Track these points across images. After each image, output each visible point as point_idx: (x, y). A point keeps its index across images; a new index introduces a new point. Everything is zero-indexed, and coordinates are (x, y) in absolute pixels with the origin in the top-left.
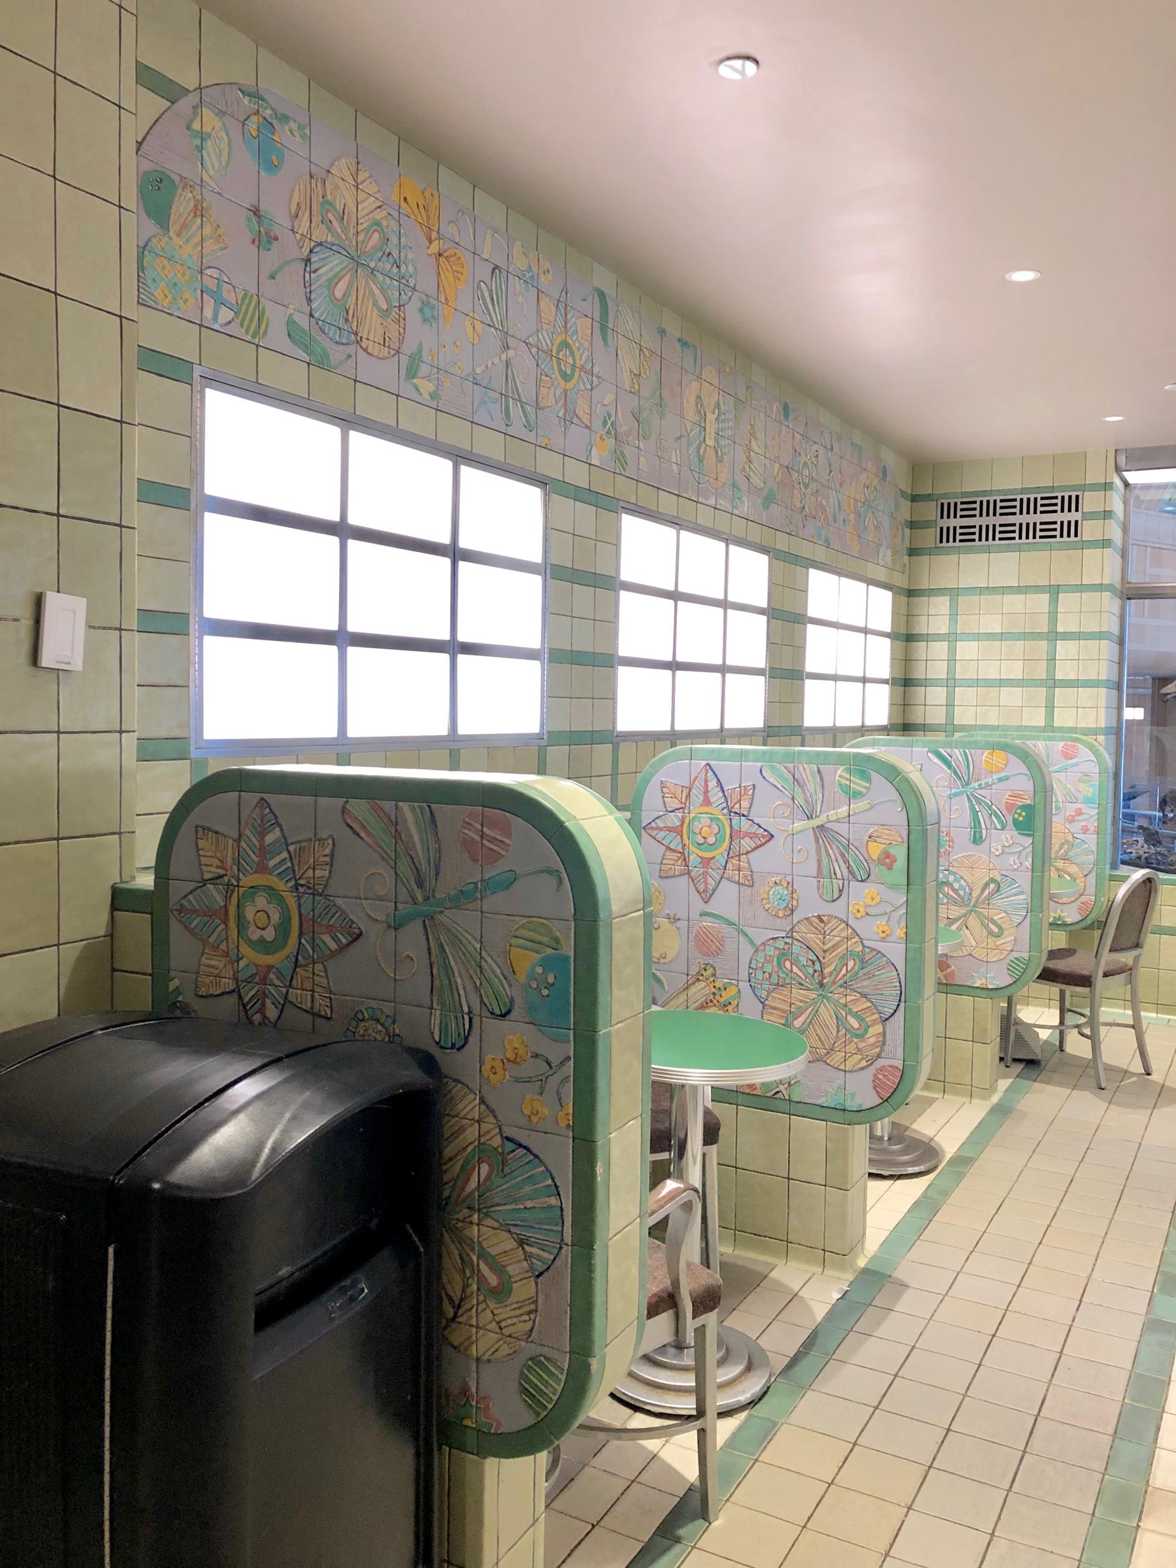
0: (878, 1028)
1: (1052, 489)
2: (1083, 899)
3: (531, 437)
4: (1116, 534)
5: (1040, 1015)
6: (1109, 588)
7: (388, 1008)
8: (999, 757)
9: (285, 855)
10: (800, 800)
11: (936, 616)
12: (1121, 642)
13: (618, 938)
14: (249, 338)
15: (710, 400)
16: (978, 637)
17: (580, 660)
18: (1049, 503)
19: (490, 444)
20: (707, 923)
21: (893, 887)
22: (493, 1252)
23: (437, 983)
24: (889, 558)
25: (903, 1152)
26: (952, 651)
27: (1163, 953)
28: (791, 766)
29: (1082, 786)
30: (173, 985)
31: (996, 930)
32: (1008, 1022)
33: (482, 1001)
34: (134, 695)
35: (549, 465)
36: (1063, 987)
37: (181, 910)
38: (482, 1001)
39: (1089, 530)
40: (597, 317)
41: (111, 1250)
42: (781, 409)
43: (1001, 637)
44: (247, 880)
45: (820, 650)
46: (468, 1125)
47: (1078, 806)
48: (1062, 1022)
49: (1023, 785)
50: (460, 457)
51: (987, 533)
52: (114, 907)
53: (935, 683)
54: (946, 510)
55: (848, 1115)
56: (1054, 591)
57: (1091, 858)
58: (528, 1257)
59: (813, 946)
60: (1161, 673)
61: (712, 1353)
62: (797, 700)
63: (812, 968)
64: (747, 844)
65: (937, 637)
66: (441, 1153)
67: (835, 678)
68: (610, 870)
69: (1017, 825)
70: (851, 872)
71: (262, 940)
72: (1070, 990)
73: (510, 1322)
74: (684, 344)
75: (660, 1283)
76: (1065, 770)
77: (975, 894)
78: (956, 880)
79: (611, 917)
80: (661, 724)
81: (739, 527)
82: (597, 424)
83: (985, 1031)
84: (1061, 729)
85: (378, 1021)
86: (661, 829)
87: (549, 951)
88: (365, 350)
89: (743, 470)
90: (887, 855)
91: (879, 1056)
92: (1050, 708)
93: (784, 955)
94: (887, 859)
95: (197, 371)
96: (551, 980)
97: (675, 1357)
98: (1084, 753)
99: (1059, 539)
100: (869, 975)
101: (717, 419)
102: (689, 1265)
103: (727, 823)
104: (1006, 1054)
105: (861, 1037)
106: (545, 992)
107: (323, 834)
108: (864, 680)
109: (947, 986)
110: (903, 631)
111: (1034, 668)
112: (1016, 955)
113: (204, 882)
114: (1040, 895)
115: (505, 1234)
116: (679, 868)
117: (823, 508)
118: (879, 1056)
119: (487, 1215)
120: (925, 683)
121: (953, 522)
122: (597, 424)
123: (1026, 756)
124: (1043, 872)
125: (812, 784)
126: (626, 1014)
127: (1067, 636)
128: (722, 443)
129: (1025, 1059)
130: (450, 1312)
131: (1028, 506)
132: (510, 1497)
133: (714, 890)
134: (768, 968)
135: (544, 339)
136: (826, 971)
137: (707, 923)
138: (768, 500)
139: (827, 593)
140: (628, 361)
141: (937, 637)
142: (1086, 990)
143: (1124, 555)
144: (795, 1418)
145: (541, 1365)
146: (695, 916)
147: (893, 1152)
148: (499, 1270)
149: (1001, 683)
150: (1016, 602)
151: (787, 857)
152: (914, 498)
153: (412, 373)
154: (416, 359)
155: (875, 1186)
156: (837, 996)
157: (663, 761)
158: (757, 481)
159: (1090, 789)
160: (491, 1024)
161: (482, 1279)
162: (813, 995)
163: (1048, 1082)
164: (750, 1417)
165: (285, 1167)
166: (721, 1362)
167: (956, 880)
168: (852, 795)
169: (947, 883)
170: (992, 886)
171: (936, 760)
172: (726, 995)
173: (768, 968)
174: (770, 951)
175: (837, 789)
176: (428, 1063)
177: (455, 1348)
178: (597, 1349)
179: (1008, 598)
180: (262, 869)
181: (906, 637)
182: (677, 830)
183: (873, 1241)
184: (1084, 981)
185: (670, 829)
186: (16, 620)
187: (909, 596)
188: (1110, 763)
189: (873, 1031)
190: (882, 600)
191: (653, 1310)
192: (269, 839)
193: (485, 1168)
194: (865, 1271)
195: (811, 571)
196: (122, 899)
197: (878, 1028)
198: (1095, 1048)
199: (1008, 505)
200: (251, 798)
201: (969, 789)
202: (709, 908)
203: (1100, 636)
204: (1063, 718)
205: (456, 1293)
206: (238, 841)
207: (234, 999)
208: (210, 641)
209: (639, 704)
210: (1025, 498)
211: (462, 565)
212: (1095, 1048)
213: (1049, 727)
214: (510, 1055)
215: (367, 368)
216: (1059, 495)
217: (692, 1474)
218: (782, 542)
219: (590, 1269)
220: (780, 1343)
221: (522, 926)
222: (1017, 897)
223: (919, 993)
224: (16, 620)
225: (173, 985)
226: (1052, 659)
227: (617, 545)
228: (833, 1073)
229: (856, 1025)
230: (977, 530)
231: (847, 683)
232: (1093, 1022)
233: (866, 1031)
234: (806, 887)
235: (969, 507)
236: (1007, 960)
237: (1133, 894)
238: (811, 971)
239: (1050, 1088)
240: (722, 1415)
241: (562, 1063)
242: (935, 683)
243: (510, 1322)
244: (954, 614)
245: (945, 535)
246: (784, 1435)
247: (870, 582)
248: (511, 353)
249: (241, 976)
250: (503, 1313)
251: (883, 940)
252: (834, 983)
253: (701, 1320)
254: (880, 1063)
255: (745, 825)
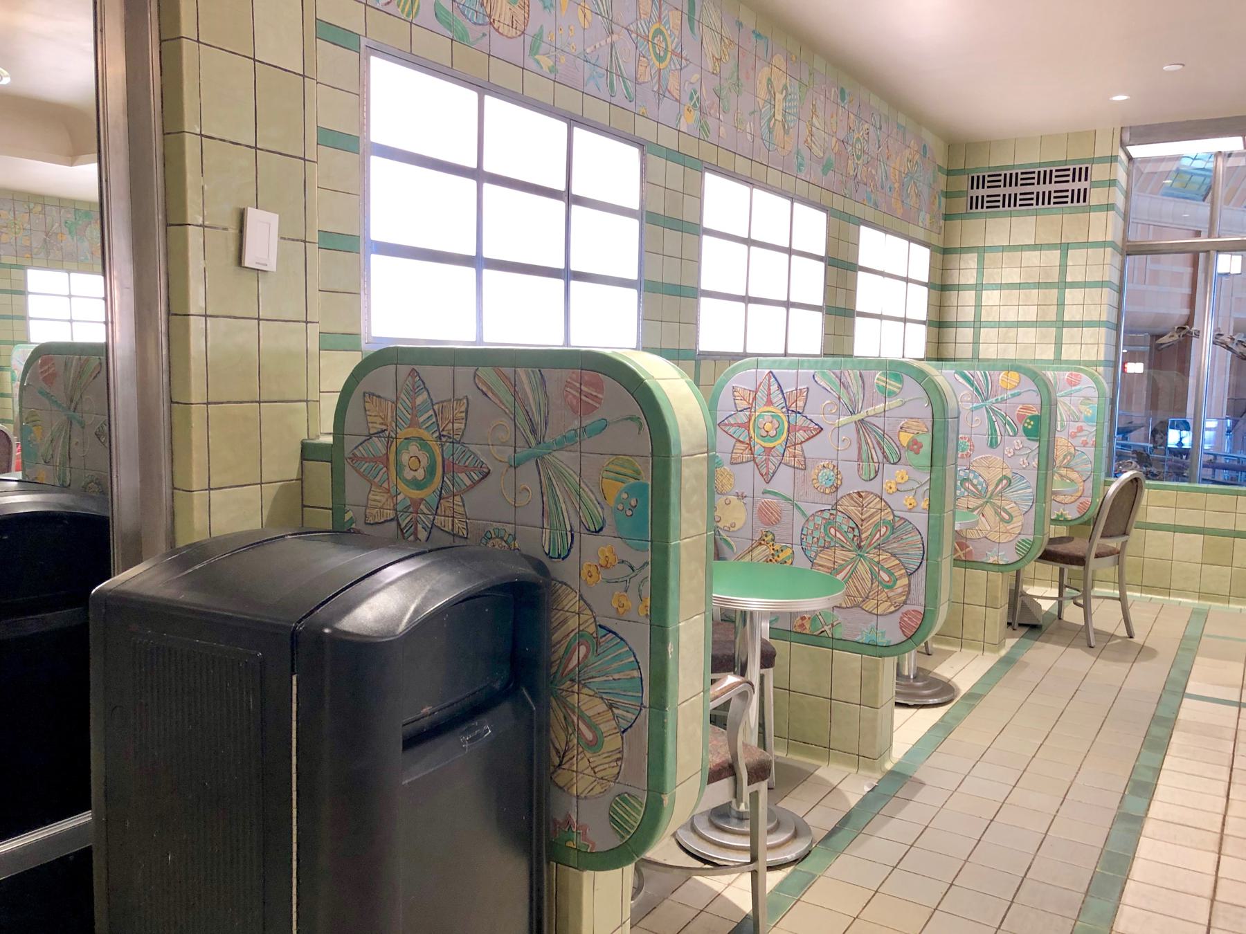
0: (905, 581)
1: (1066, 162)
2: (1082, 500)
3: (631, 106)
4: (1120, 201)
5: (1043, 593)
6: (1112, 244)
7: (509, 528)
8: (1014, 376)
9: (431, 412)
10: (845, 399)
11: (966, 270)
12: (1120, 291)
13: (686, 472)
14: (404, 16)
15: (778, 84)
16: (1000, 286)
17: (669, 291)
18: (1063, 174)
19: (599, 111)
20: (769, 499)
21: (918, 468)
22: (590, 713)
23: (546, 507)
24: (928, 222)
25: (924, 688)
26: (979, 298)
27: (1146, 544)
28: (838, 372)
29: (1082, 408)
30: (347, 517)
31: (1006, 517)
32: (1016, 598)
33: (581, 521)
34: (316, 298)
35: (644, 129)
36: (1062, 565)
37: (354, 458)
38: (581, 521)
39: (1096, 197)
40: (686, 10)
41: (294, 678)
42: (838, 93)
43: (1019, 286)
44: (402, 433)
45: (869, 293)
46: (570, 618)
47: (1080, 424)
48: (1061, 594)
49: (1031, 399)
50: (573, 121)
51: (1009, 201)
52: (304, 458)
53: (964, 324)
54: (976, 182)
55: (880, 650)
56: (1064, 248)
57: (1089, 467)
58: (616, 717)
59: (853, 516)
60: (1159, 330)
61: (763, 825)
62: (849, 333)
63: (852, 534)
64: (801, 435)
65: (967, 287)
66: (549, 639)
67: (880, 317)
68: (680, 419)
69: (1027, 433)
70: (885, 457)
71: (415, 479)
72: (1068, 568)
73: (601, 767)
74: (758, 36)
75: (721, 756)
76: (1070, 395)
77: (990, 489)
78: (975, 477)
79: (680, 456)
80: (739, 349)
81: (802, 188)
82: (685, 98)
83: (996, 598)
84: (1067, 362)
85: (502, 538)
86: (732, 425)
87: (632, 481)
88: (497, 30)
89: (806, 141)
90: (915, 442)
91: (905, 603)
92: (1059, 344)
93: (830, 523)
94: (915, 446)
95: (364, 42)
96: (633, 502)
97: (737, 825)
98: (1086, 381)
99: (1069, 204)
100: (898, 539)
101: (785, 98)
102: (745, 745)
103: (785, 419)
104: (1014, 618)
105: (891, 588)
106: (629, 513)
107: (459, 395)
108: (905, 320)
109: (965, 562)
110: (938, 282)
111: (1047, 317)
112: (1023, 537)
113: (370, 436)
114: (1043, 492)
115: (597, 701)
116: (747, 456)
117: (873, 177)
118: (905, 603)
119: (585, 686)
120: (956, 324)
121: (981, 192)
122: (685, 98)
123: (1035, 377)
124: (1047, 469)
125: (855, 386)
126: (692, 532)
127: (1074, 285)
128: (789, 118)
129: (1027, 623)
130: (557, 761)
131: (1045, 177)
132: (602, 906)
133: (774, 473)
134: (816, 534)
135: (642, 27)
136: (863, 536)
137: (769, 499)
138: (827, 168)
139: (875, 247)
140: (712, 48)
141: (967, 287)
142: (1081, 568)
143: (1126, 217)
144: (829, 872)
145: (624, 800)
146: (758, 493)
147: (918, 688)
148: (592, 727)
149: (1018, 324)
150: (1032, 258)
151: (834, 446)
152: (949, 173)
153: (534, 50)
154: (538, 37)
155: (899, 712)
156: (872, 555)
157: (734, 371)
158: (817, 151)
159: (1089, 411)
160: (589, 539)
161: (580, 735)
162: (852, 555)
163: (1047, 642)
164: (795, 870)
165: (423, 628)
166: (770, 832)
167: (975, 477)
168: (887, 394)
169: (968, 480)
170: (1004, 482)
171: (961, 380)
172: (783, 556)
173: (816, 534)
174: (819, 521)
175: (876, 389)
176: (540, 567)
177: (561, 788)
178: (668, 786)
179: (1026, 254)
180: (413, 424)
181: (940, 287)
182: (746, 426)
183: (898, 751)
184: (1080, 561)
185: (740, 425)
186: (225, 229)
187: (943, 254)
188: (1107, 388)
189: (899, 583)
190: (921, 256)
191: (715, 775)
192: (419, 401)
193: (583, 649)
194: (891, 773)
195: (862, 228)
196: (309, 452)
197: (905, 581)
198: (1087, 615)
199: (1027, 177)
200: (404, 370)
201: (988, 403)
202: (769, 488)
203: (1101, 284)
204: (1069, 353)
205: (561, 746)
206: (395, 403)
207: (394, 524)
208: (375, 258)
209: (717, 329)
210: (1042, 170)
211: (574, 208)
212: (1087, 615)
213: (1058, 359)
214: (603, 562)
215: (499, 45)
216: (1072, 168)
217: (748, 908)
218: (838, 203)
219: (663, 726)
220: (821, 820)
221: (612, 463)
222: (1024, 492)
223: (939, 552)
224: (225, 229)
225: (347, 517)
226: (1061, 304)
227: (701, 199)
228: (868, 616)
229: (887, 579)
230: (1001, 198)
231: (891, 326)
232: (1086, 596)
233: (895, 583)
234: (849, 470)
235: (995, 179)
236: (1015, 542)
237: (1122, 490)
238: (851, 536)
239: (1049, 646)
240: (770, 868)
241: (642, 567)
242: (964, 324)
243: (601, 767)
244: (981, 269)
245: (975, 203)
246: (821, 882)
247: (911, 240)
248: (615, 37)
249: (399, 508)
250: (596, 760)
251: (910, 511)
252: (870, 545)
253: (755, 787)
254: (906, 608)
255: (800, 420)
